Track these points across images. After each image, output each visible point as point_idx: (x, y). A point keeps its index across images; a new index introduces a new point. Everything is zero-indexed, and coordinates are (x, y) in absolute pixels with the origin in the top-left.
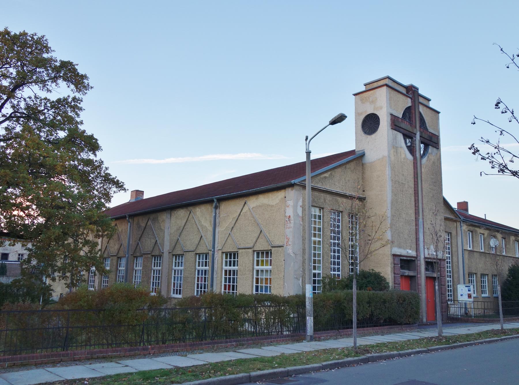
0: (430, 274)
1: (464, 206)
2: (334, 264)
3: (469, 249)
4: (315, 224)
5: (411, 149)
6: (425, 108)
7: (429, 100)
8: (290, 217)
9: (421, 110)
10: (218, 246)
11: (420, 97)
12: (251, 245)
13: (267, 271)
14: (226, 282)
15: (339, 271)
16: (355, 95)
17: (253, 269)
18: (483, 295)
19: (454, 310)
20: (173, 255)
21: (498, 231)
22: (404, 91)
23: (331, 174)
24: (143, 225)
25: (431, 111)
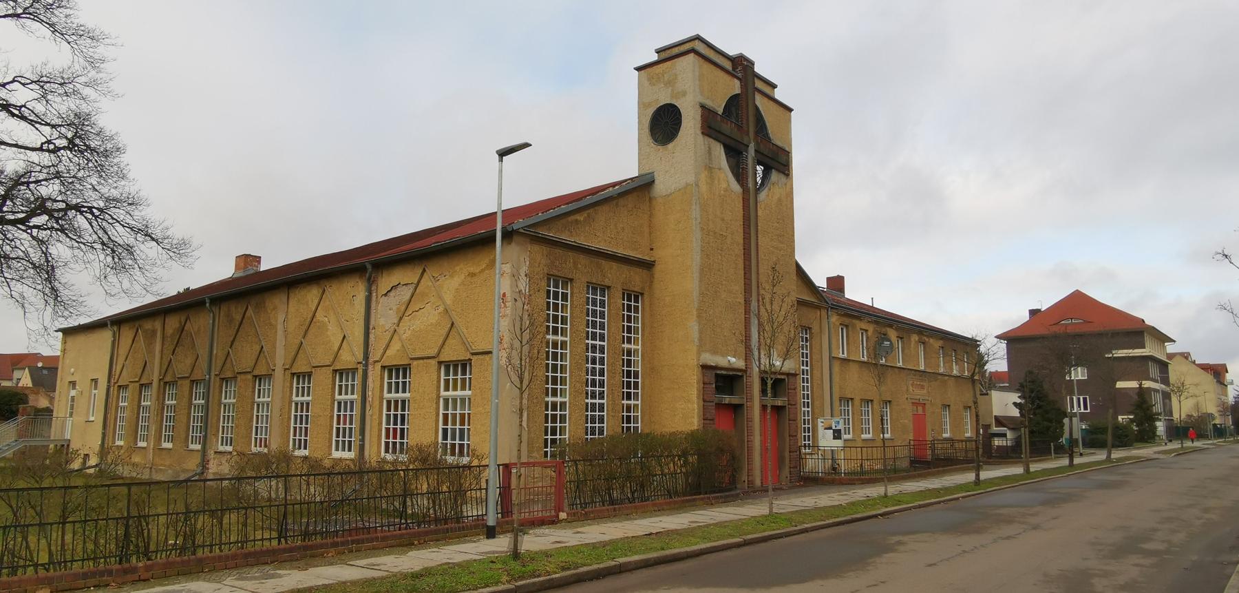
0: (770, 401)
1: (837, 283)
2: (593, 385)
3: (841, 355)
4: (556, 309)
5: (739, 173)
6: (766, 100)
7: (774, 86)
8: (504, 295)
9: (758, 103)
10: (375, 355)
11: (756, 80)
12: (433, 352)
13: (463, 400)
14: (388, 423)
15: (603, 398)
16: (639, 69)
17: (438, 397)
18: (864, 436)
19: (813, 464)
20: (293, 374)
21: (891, 326)
22: (728, 65)
23: (589, 215)
24: (238, 317)
25: (775, 106)
